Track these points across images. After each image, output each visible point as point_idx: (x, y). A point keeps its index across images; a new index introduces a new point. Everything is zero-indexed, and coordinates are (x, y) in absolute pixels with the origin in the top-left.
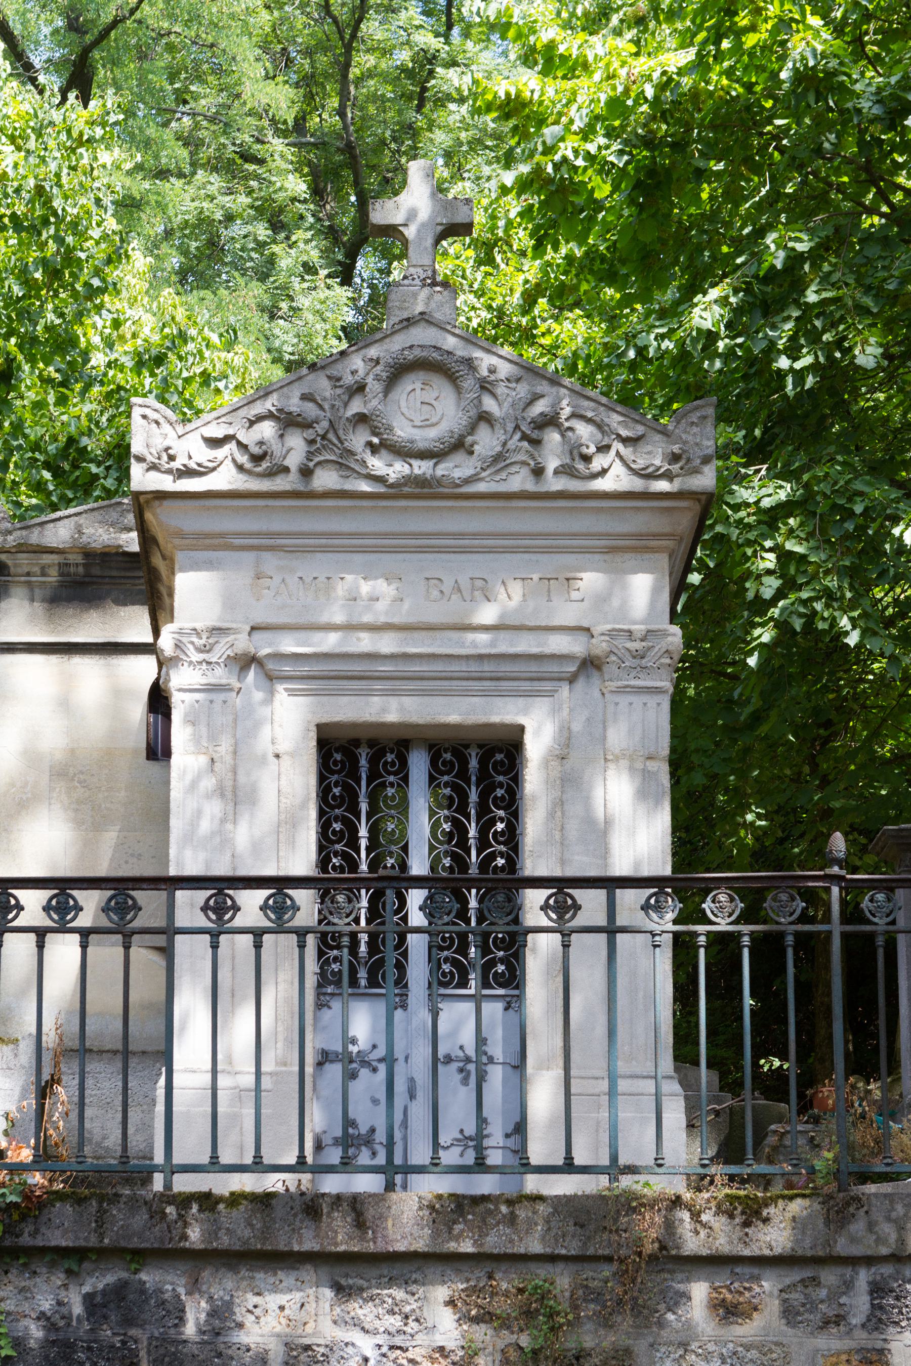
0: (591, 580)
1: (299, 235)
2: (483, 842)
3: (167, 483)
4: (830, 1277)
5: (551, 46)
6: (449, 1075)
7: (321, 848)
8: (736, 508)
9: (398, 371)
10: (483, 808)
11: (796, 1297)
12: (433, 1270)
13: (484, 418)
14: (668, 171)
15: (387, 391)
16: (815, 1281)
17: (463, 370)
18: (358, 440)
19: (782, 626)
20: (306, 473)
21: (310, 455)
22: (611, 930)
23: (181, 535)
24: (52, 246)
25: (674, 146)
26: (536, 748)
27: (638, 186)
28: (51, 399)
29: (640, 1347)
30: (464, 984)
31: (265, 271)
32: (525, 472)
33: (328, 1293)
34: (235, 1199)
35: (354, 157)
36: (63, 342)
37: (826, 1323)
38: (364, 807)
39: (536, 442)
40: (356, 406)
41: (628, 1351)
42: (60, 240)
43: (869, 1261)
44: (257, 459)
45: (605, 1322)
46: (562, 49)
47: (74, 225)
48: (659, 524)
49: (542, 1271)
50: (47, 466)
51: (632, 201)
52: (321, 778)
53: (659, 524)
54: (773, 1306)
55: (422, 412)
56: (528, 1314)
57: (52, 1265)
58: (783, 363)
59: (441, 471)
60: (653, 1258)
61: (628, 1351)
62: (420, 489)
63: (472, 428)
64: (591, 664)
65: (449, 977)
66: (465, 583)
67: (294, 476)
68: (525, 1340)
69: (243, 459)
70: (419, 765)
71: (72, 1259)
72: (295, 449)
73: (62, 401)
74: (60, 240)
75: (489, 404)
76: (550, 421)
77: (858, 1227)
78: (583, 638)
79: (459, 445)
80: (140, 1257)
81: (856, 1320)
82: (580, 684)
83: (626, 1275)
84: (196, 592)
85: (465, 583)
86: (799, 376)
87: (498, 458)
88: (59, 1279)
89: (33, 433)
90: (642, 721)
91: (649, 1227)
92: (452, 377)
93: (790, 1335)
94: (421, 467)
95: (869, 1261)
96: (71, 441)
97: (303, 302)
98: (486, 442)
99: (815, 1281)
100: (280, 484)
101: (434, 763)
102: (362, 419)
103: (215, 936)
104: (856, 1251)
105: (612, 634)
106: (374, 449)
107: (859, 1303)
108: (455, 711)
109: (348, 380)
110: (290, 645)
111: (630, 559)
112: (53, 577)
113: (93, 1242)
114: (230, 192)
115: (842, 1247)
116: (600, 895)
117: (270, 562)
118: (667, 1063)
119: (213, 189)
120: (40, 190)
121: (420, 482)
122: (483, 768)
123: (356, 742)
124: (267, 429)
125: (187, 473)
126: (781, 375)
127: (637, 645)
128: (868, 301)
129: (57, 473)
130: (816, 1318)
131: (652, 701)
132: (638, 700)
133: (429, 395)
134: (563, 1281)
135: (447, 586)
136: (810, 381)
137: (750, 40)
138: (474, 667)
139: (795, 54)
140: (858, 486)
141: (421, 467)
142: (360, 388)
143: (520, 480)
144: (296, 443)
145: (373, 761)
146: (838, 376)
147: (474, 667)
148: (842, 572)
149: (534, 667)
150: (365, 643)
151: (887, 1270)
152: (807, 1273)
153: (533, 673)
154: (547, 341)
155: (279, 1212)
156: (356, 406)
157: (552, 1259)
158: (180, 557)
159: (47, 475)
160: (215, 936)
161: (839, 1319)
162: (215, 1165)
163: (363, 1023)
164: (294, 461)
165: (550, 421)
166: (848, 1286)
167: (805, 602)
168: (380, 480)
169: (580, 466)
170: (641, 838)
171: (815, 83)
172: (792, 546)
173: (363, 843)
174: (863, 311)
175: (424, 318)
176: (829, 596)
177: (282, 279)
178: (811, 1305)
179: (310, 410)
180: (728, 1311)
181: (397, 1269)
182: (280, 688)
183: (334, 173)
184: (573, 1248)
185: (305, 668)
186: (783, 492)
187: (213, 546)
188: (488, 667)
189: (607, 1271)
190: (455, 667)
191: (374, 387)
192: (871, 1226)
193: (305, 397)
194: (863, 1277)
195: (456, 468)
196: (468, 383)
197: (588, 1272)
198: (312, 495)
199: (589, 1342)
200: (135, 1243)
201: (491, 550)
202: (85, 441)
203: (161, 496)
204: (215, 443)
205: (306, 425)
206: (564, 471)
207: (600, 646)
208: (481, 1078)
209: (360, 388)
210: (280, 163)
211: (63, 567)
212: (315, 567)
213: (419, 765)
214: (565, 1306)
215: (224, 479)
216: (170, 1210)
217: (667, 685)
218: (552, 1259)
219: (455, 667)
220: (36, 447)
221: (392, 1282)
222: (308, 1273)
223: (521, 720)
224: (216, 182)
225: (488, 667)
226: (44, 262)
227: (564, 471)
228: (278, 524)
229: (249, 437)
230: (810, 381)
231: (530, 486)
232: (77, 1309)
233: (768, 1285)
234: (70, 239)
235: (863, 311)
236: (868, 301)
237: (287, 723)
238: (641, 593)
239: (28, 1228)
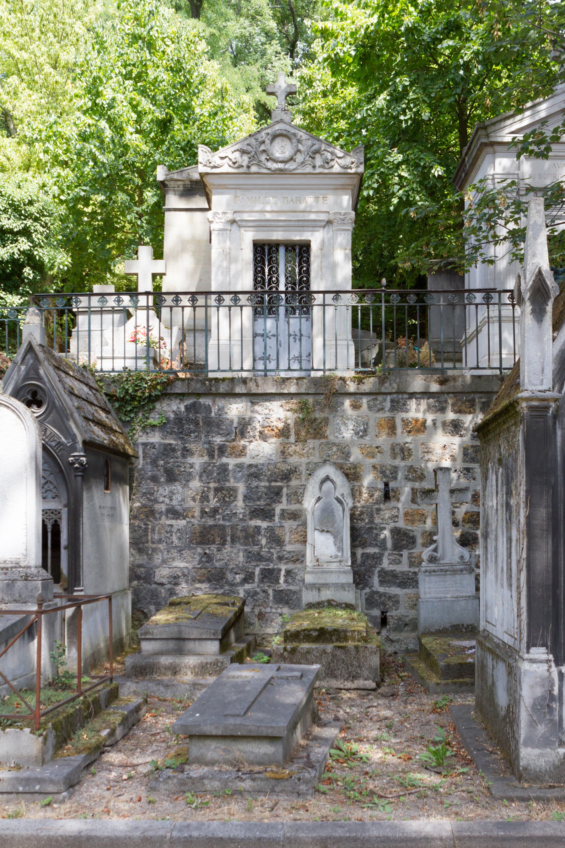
0: (331, 198)
1: (274, 42)
2: (300, 273)
3: (209, 170)
4: (380, 398)
5: (337, 9)
6: (291, 338)
7: (255, 275)
8: (387, 163)
9: (275, 137)
10: (300, 264)
11: (371, 403)
12: (277, 398)
13: (299, 151)
14: (369, 54)
15: (271, 142)
16: (376, 399)
17: (293, 137)
18: (263, 157)
19: (400, 198)
20: (248, 167)
21: (249, 162)
22: (324, 305)
23: (213, 185)
24: (182, 78)
25: (371, 47)
26: (314, 247)
27: (361, 59)
28: (183, 128)
29: (331, 417)
30: (295, 314)
31: (263, 54)
32: (310, 167)
33: (249, 404)
34: (224, 380)
35: (293, 12)
36: (187, 107)
37: (379, 410)
38: (267, 263)
39: (313, 158)
40: (263, 147)
41: (328, 418)
42: (185, 76)
43: (390, 394)
44: (234, 163)
45: (322, 410)
46: (340, 10)
47: (189, 72)
48: (348, 182)
49: (305, 397)
50: (182, 149)
51: (359, 64)
52: (255, 255)
53: (348, 182)
54: (365, 406)
55: (281, 150)
56: (302, 409)
57: (176, 398)
58: (402, 118)
59: (287, 166)
60: (334, 394)
61: (328, 418)
62: (281, 172)
63: (295, 154)
64: (329, 222)
65: (291, 311)
66: (294, 199)
67: (245, 168)
68: (301, 416)
69: (231, 163)
70: (282, 250)
71: (181, 396)
72: (245, 160)
73: (186, 128)
74: (185, 76)
75: (300, 147)
76: (317, 152)
77: (387, 385)
78: (327, 215)
79: (291, 159)
80: (199, 395)
81: (387, 409)
82: (326, 229)
83: (327, 398)
84: (219, 200)
85: (294, 199)
86: (406, 121)
87: (302, 163)
88: (178, 401)
89: (178, 138)
90: (344, 239)
91: (337, 385)
92: (290, 139)
93: (370, 413)
94: (280, 166)
95: (390, 394)
96: (189, 142)
97: (275, 64)
98: (299, 158)
99: (376, 399)
100: (241, 170)
101: (286, 250)
102: (264, 151)
103: (218, 308)
104: (387, 391)
105: (335, 213)
106: (267, 160)
107: (388, 405)
108: (297, 237)
109: (260, 139)
110: (246, 217)
111: (341, 192)
112: (181, 188)
113: (186, 391)
114: (251, 25)
115: (383, 390)
116: (321, 295)
117: (239, 192)
118: (350, 337)
119: (245, 25)
120: (178, 61)
121: (280, 170)
122: (302, 250)
123: (264, 245)
124: (237, 154)
125: (215, 167)
126: (401, 121)
127: (342, 217)
128: (426, 99)
129: (184, 151)
130: (376, 409)
131: (347, 233)
132: (343, 233)
133: (283, 144)
134: (311, 400)
135: (289, 200)
136: (410, 122)
137: (393, 14)
138: (297, 223)
139: (405, 22)
140: (422, 156)
141: (280, 166)
142: (264, 142)
143: (309, 169)
144: (246, 158)
145: (269, 250)
146: (417, 122)
147: (297, 223)
148: (417, 182)
149: (313, 223)
150: (268, 216)
151: (395, 396)
152: (374, 397)
153: (314, 225)
154: (342, 95)
155: (236, 382)
156: (263, 147)
157: (308, 394)
158: (213, 191)
159: (182, 152)
160: (218, 308)
161: (382, 409)
162: (219, 370)
163: (270, 323)
164: (245, 164)
165: (317, 152)
166: (385, 400)
167: (407, 191)
168: (269, 169)
169: (326, 165)
170: (344, 271)
171: (410, 31)
172: (403, 174)
173: (267, 274)
174: (424, 102)
175: (282, 121)
176: (413, 189)
177: (268, 57)
178: (375, 405)
179: (249, 149)
180: (355, 407)
181: (267, 397)
182: (242, 229)
183: (287, 17)
184: (312, 391)
185: (255, 224)
186: (400, 158)
187: (224, 188)
188: (300, 223)
189: (322, 397)
190: (291, 223)
191: (267, 142)
192: (390, 384)
193: (248, 145)
194: (389, 398)
195: (290, 166)
196: (294, 140)
197: (317, 397)
198: (250, 174)
199: (317, 416)
200: (198, 392)
201: (302, 189)
202: (193, 142)
203: (207, 174)
204: (222, 158)
205: (249, 153)
206: (322, 167)
207: (332, 217)
208: (300, 340)
209: (264, 142)
210: (268, 16)
211: (184, 185)
212: (254, 194)
213: (282, 250)
214: (311, 406)
215: (226, 169)
216: (207, 383)
217: (350, 228)
218: (308, 394)
219: (291, 223)
220: (178, 143)
221: (266, 401)
222: (244, 399)
223: (310, 238)
224: (247, 23)
225: (300, 223)
226: (180, 83)
227: (322, 167)
228: (241, 182)
229: (232, 156)
230: (410, 122)
231: (312, 171)
232: (183, 409)
233: (365, 400)
234: (188, 76)
235: (424, 102)
236: (426, 99)
237: (248, 237)
238: (346, 200)
239: (169, 388)
